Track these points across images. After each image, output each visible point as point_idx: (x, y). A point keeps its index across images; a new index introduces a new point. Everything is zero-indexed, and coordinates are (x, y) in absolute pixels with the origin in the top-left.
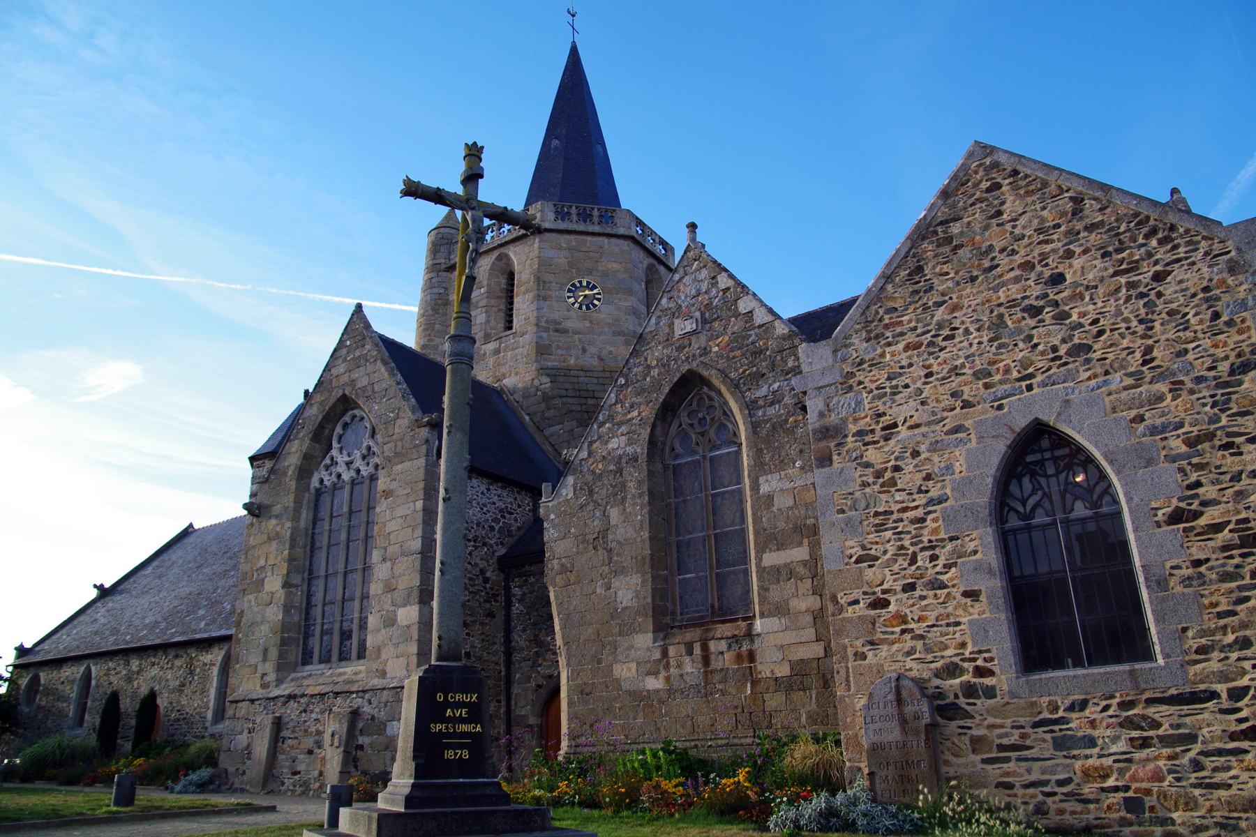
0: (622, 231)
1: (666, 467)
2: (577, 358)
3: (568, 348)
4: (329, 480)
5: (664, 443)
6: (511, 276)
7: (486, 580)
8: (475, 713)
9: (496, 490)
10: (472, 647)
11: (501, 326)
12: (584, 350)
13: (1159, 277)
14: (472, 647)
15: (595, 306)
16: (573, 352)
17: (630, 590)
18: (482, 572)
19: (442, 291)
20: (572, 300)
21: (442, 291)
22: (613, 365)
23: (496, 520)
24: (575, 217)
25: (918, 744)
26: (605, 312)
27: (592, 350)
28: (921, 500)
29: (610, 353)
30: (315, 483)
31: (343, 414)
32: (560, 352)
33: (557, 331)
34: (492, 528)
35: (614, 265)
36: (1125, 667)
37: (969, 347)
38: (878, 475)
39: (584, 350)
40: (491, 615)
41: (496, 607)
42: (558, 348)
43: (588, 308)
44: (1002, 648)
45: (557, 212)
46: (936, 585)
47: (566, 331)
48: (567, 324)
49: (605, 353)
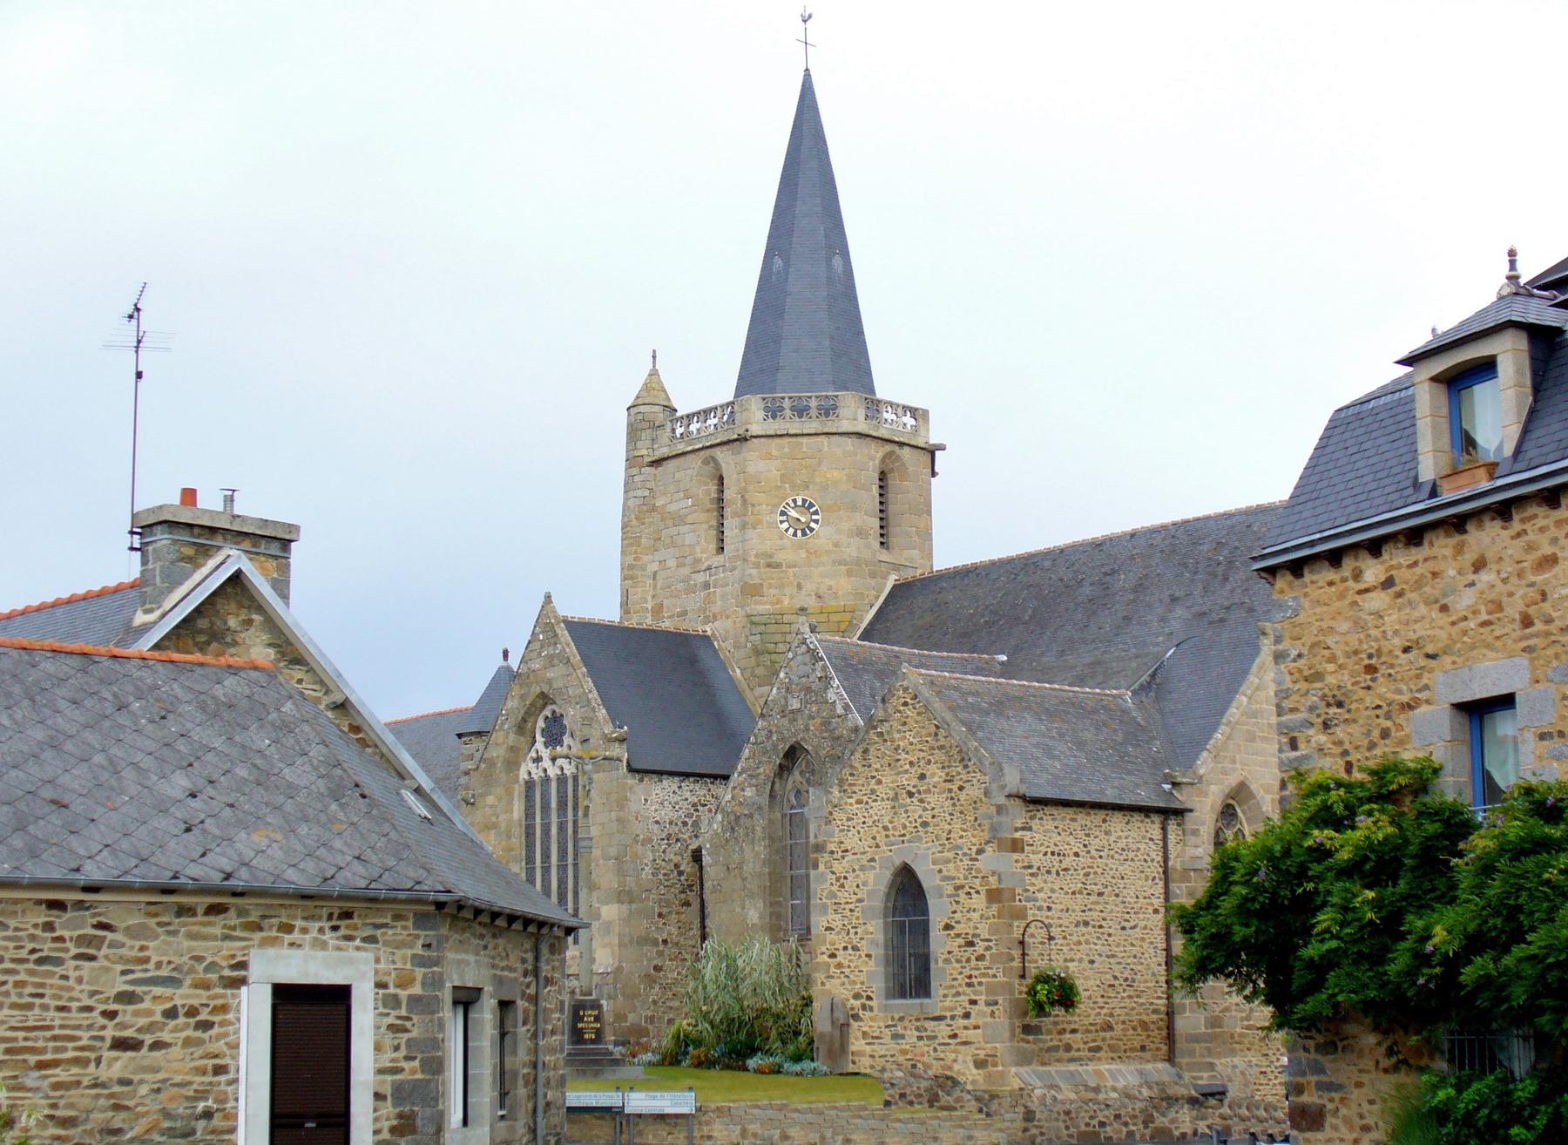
0: (845, 426)
1: (784, 816)
2: (792, 597)
3: (781, 586)
4: (537, 774)
5: (782, 796)
6: (721, 479)
7: (681, 873)
8: (597, 1019)
9: (688, 785)
10: (670, 934)
11: (713, 547)
12: (799, 587)
13: (961, 788)
14: (670, 934)
15: (812, 530)
16: (787, 591)
17: (754, 914)
18: (676, 866)
19: (647, 493)
20: (785, 525)
21: (647, 493)
22: (834, 603)
23: (689, 816)
24: (788, 412)
25: (837, 1033)
26: (823, 533)
27: (809, 586)
28: (854, 898)
29: (830, 588)
30: (523, 776)
31: (544, 707)
32: (773, 591)
33: (769, 565)
34: (685, 824)
35: (836, 474)
36: (918, 1001)
37: (880, 809)
38: (838, 879)
39: (799, 587)
40: (687, 904)
41: (692, 897)
42: (770, 586)
43: (804, 534)
44: (878, 986)
45: (766, 409)
46: (855, 948)
47: (779, 566)
48: (780, 557)
49: (823, 590)
